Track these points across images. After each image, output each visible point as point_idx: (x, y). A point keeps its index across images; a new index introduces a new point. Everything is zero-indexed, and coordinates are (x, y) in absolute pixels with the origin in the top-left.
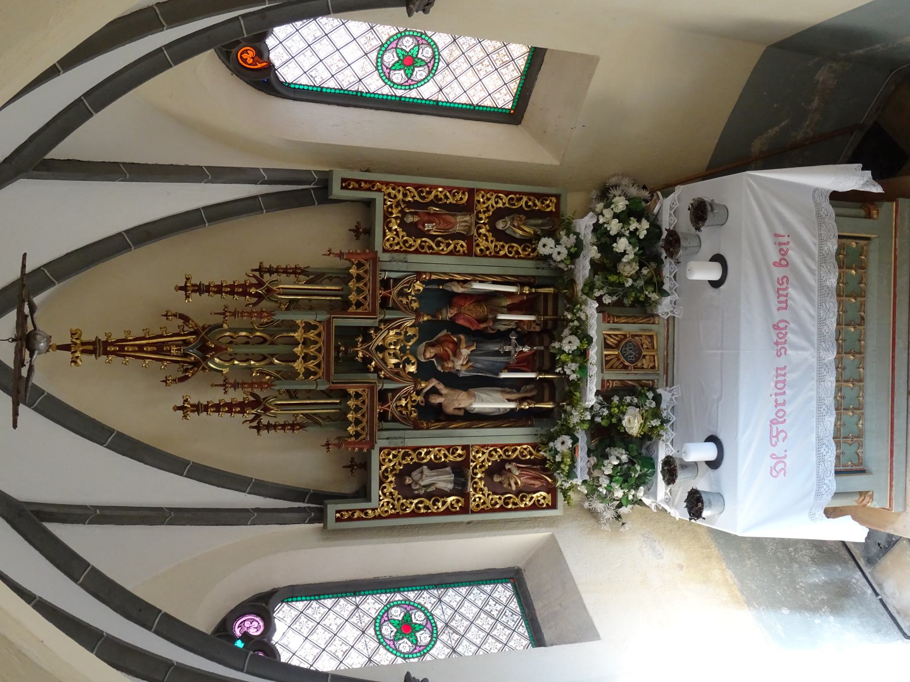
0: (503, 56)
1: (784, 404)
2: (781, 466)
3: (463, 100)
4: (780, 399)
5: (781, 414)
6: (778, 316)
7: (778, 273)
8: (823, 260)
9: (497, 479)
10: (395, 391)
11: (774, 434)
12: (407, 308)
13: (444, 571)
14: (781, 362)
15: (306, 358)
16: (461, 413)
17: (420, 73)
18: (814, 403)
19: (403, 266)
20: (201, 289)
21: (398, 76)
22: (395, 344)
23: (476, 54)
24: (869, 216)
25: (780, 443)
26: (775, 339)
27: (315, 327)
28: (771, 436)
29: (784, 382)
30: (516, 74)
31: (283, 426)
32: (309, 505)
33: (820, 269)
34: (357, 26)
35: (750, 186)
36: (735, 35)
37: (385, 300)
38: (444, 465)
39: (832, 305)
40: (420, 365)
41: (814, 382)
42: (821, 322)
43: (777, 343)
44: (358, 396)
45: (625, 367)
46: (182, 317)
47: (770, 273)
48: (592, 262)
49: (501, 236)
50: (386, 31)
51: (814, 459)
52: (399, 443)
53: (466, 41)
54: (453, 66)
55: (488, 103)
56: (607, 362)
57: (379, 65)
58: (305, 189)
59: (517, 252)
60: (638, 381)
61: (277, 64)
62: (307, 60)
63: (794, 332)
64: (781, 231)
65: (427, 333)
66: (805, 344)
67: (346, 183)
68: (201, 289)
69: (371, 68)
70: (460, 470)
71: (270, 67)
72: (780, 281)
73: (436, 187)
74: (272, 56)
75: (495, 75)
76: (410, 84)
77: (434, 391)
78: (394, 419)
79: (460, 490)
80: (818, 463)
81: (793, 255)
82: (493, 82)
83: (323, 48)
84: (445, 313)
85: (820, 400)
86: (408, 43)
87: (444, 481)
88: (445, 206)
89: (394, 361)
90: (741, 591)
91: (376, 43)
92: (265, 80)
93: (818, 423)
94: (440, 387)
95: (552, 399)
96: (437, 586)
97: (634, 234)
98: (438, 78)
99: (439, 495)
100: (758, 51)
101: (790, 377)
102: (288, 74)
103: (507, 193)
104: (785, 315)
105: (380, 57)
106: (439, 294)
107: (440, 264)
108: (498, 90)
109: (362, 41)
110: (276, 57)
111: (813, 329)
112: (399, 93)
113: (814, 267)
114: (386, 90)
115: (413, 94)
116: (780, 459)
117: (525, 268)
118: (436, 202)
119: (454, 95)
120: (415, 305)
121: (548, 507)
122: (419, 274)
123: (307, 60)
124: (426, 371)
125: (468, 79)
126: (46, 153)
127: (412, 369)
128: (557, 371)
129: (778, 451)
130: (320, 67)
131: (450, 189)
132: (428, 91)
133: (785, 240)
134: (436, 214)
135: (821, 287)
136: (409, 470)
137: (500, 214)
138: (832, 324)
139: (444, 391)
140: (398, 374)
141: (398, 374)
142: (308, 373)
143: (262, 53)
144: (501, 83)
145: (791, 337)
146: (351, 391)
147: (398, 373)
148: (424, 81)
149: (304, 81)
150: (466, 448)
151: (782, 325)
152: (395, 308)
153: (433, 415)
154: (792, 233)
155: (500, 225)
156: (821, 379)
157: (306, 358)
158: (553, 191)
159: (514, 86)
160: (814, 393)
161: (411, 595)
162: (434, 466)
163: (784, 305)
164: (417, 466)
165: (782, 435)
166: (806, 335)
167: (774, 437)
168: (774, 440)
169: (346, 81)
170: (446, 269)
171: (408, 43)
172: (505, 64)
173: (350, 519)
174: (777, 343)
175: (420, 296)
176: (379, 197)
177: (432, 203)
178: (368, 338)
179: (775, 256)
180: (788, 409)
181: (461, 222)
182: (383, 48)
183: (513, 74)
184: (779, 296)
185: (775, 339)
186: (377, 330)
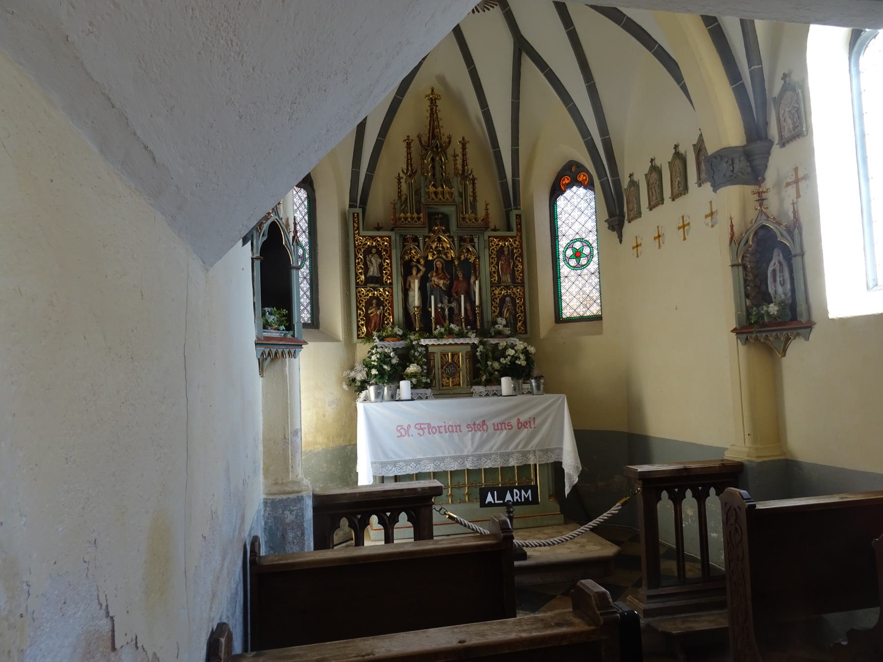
0: (588, 302)
1: (440, 432)
2: (403, 433)
3: (563, 291)
4: (442, 429)
5: (434, 430)
6: (489, 424)
7: (514, 422)
8: (525, 454)
9: (374, 301)
10: (418, 246)
11: (423, 426)
12: (461, 253)
13: (320, 287)
14: (464, 429)
15: (436, 193)
16: (407, 287)
17: (573, 262)
18: (441, 455)
19: (482, 246)
20: (464, 148)
21: (569, 253)
22: (443, 247)
23: (587, 289)
24: (550, 496)
25: (417, 431)
26: (477, 422)
27: (451, 197)
28: (421, 424)
29: (453, 431)
30: (581, 314)
31: (399, 188)
32: (359, 199)
33: (518, 452)
34: (591, 224)
35: (558, 399)
36: (632, 406)
37: (464, 240)
38: (382, 273)
39: (498, 464)
40: (432, 261)
41: (453, 454)
42: (487, 456)
43: (474, 424)
44: (419, 218)
45: (442, 368)
46: (450, 142)
47: (513, 416)
48: (497, 344)
49: (503, 300)
50: (592, 238)
51: (408, 458)
52: (393, 246)
53: (595, 280)
54: (580, 278)
55: (564, 305)
56: (444, 355)
57: (574, 241)
58: (511, 198)
59: (494, 312)
60: (435, 376)
61: (565, 195)
62: (569, 209)
63: (482, 435)
64: (537, 421)
65: (449, 264)
66: (475, 445)
67: (519, 217)
68: (464, 148)
69: (571, 238)
70: (377, 281)
71: (562, 192)
72: (509, 425)
73: (522, 265)
74: (568, 191)
75: (578, 304)
76: (567, 260)
77: (419, 270)
78: (404, 246)
79: (369, 280)
80: (405, 461)
81: (525, 432)
82: (574, 303)
83: (576, 214)
84: (460, 273)
85: (443, 459)
86: (587, 251)
87: (373, 271)
88: (513, 270)
89: (434, 247)
90: (310, 451)
91: (584, 236)
92: (556, 191)
93: (427, 459)
94: (421, 273)
95: (420, 330)
96: (311, 279)
97: (518, 358)
98: (573, 273)
99: (366, 270)
100: (624, 429)
101: (455, 435)
102: (561, 202)
103: (524, 304)
104: (491, 430)
105: (577, 240)
106: (470, 269)
107: (485, 268)
108: (571, 308)
109: (584, 229)
110: (568, 193)
111: (485, 450)
112: (561, 257)
113: (520, 447)
114: (561, 249)
115: (562, 263)
116: (407, 432)
117: (488, 316)
118: (515, 266)
119: (565, 285)
120: (463, 258)
121: (358, 335)
122: (479, 258)
123: (569, 209)
124: (429, 265)
125: (574, 290)
126: (527, 54)
127: (430, 258)
128: (436, 332)
129: (413, 431)
130: (567, 215)
131: (522, 272)
132: (564, 270)
133: (533, 426)
134: (509, 263)
135: (509, 455)
136: (379, 253)
137: (513, 300)
138: (488, 465)
139: (419, 275)
140: (427, 248)
141: (427, 248)
142: (428, 193)
143: (569, 186)
144: (575, 307)
145: (479, 433)
146: (421, 215)
147: (428, 248)
148: (569, 266)
149: (559, 210)
150: (391, 284)
151: (485, 427)
152: (460, 246)
153: (407, 269)
154: (537, 430)
155: (508, 299)
156: (455, 458)
157: (436, 193)
158: (528, 329)
159: (575, 315)
160: (446, 455)
161: (308, 263)
162: (381, 267)
163: (498, 427)
164: (381, 257)
165: (421, 432)
166: (482, 443)
167: (420, 427)
168: (418, 426)
169: (562, 228)
170: (482, 271)
171: (587, 251)
172: (585, 306)
173: (354, 221)
174: (474, 424)
175: (467, 260)
176: (514, 233)
177: (514, 263)
178: (444, 232)
179: (523, 418)
180: (437, 435)
181: (507, 279)
182: (581, 240)
183: (582, 311)
184: (501, 424)
185: (477, 422)
186: (449, 237)
